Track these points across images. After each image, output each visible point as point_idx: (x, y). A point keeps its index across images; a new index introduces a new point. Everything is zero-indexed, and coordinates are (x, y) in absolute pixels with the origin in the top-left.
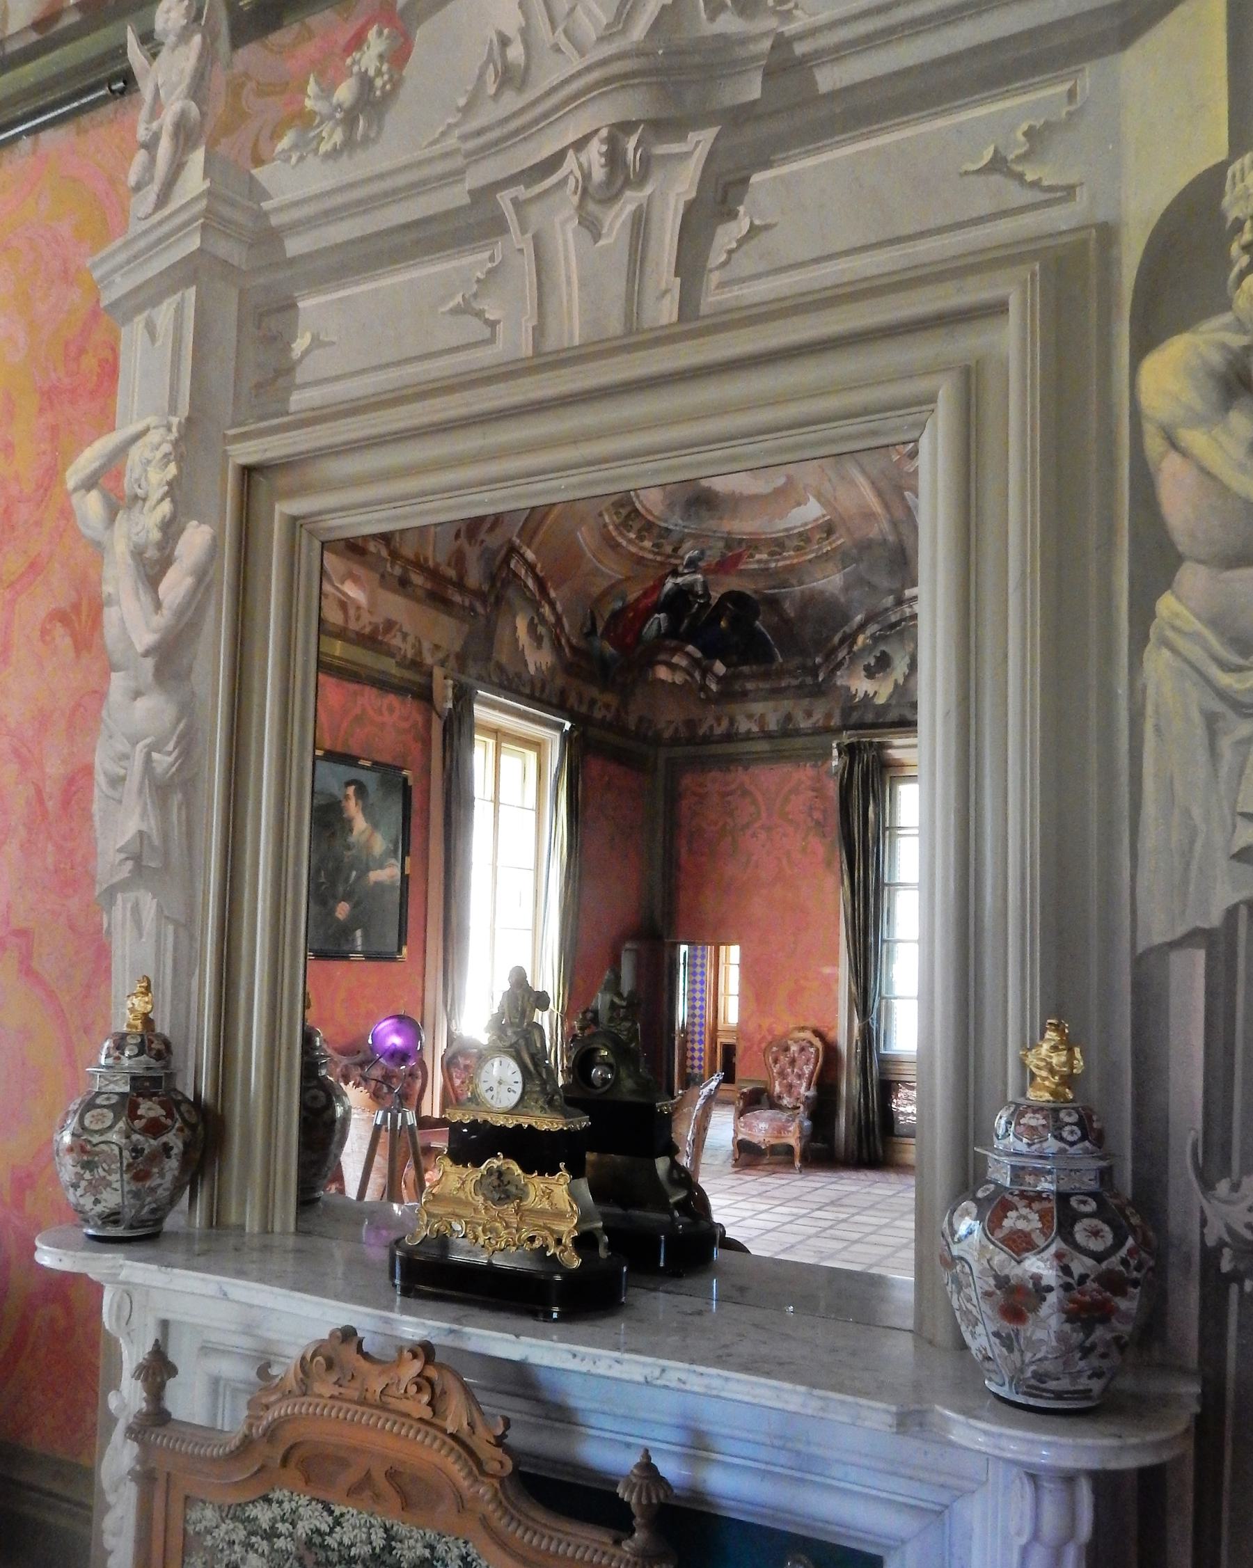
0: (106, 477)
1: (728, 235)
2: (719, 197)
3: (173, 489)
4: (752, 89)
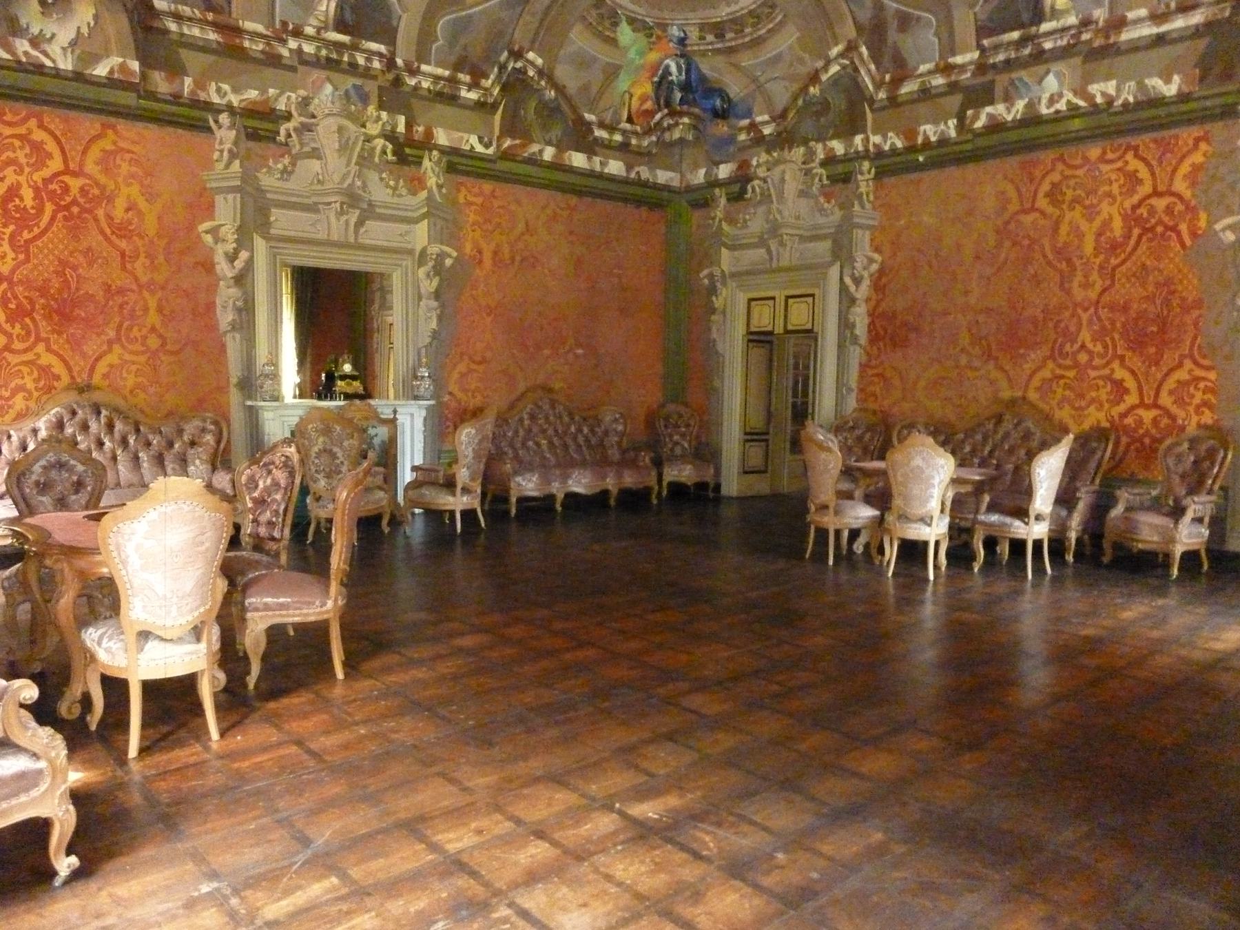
0: (214, 231)
1: (362, 230)
2: (360, 223)
3: (237, 241)
4: (365, 206)
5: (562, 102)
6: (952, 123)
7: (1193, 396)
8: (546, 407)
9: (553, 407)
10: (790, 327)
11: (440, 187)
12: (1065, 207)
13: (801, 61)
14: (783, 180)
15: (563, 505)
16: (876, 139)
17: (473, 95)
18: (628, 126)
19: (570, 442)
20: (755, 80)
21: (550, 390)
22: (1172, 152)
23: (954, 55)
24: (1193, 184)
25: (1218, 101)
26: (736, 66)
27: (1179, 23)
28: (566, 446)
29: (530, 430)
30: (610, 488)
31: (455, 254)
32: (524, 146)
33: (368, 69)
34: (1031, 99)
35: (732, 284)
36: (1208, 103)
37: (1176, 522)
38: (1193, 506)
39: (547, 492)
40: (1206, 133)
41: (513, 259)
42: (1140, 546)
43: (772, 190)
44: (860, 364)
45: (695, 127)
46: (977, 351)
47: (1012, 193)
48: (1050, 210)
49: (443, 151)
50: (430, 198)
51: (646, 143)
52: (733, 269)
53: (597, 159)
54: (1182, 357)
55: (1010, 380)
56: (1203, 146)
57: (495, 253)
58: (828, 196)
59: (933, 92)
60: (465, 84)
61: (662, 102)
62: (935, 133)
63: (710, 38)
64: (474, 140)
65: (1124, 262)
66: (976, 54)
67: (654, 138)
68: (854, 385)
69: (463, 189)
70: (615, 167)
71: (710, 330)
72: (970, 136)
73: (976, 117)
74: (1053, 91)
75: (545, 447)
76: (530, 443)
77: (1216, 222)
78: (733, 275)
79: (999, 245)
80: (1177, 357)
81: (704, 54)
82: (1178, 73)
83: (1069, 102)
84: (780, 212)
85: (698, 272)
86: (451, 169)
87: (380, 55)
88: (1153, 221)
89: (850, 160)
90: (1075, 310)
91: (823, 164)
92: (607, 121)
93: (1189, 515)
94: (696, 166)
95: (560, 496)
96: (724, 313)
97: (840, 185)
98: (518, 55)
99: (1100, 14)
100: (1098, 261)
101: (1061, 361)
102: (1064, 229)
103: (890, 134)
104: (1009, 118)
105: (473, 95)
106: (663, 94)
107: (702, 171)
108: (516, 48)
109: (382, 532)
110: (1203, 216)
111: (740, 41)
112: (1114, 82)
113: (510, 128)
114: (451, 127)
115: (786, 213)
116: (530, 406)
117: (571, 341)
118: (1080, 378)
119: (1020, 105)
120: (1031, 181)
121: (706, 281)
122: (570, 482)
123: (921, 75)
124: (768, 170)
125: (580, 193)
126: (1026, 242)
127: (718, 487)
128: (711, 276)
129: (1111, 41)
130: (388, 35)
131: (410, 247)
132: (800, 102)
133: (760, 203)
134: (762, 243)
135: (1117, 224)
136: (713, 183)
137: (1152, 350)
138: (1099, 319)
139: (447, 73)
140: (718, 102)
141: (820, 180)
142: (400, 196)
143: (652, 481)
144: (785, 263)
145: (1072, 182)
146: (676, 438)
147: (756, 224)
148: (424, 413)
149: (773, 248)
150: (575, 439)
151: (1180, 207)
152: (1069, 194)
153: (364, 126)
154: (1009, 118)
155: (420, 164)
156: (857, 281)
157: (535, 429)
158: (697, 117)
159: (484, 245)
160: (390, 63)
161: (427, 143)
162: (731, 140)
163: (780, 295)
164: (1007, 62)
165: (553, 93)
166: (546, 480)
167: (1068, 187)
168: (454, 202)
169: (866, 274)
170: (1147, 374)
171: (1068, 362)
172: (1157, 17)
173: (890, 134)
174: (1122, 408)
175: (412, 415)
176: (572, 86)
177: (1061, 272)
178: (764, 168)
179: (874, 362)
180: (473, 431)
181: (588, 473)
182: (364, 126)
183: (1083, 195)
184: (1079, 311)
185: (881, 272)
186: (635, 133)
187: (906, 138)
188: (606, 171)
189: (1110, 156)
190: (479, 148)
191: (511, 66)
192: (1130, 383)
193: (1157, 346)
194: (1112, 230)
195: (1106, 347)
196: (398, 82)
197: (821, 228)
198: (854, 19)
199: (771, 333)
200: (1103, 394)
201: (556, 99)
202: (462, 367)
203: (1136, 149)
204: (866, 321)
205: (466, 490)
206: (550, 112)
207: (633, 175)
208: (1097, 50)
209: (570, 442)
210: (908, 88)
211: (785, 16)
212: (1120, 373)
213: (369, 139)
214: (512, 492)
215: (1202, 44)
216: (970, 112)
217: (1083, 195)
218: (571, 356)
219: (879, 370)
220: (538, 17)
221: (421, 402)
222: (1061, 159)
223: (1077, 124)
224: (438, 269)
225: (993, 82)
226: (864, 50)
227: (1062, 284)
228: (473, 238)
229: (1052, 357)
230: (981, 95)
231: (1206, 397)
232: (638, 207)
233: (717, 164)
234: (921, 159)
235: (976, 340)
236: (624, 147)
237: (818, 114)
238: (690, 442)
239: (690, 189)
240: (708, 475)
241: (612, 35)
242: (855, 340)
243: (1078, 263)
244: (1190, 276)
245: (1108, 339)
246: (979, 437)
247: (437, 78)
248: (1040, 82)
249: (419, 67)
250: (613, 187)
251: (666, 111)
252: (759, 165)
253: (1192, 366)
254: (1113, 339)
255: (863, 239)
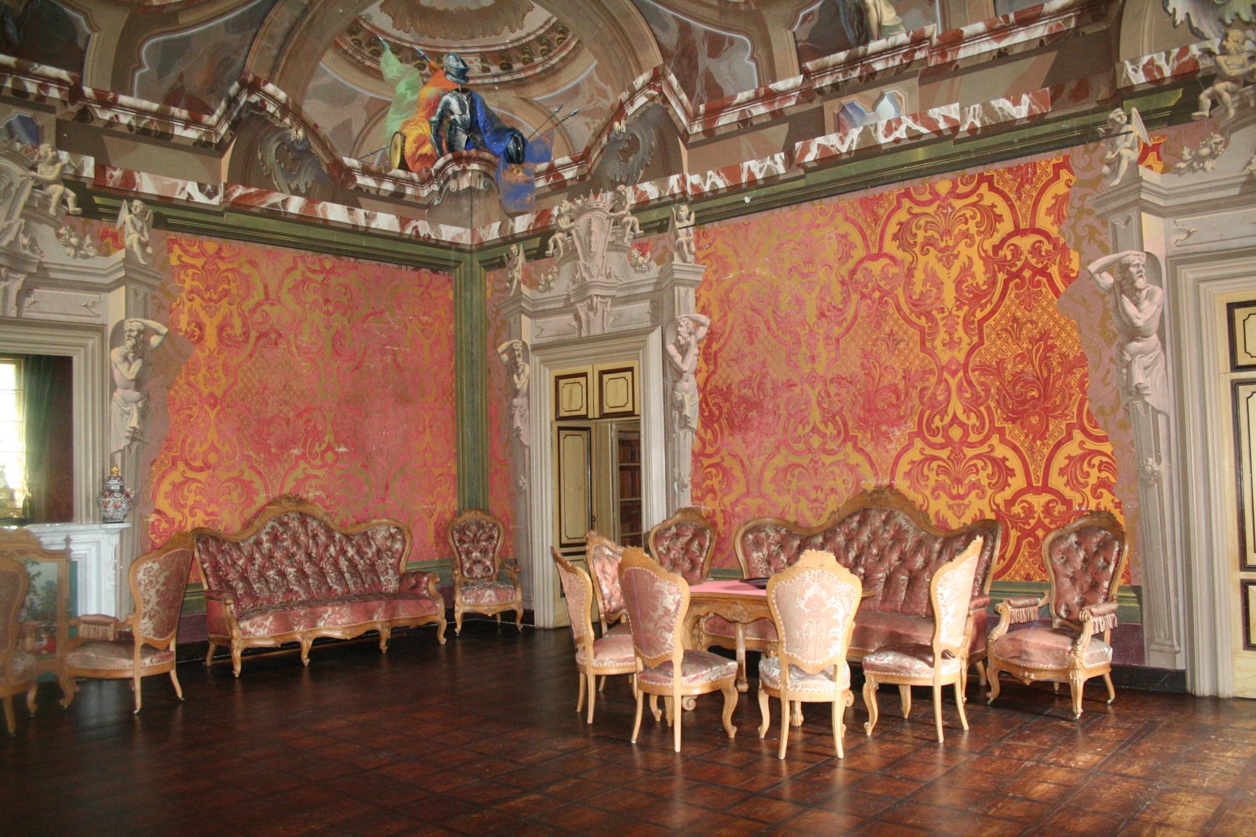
1: (28, 301)
2: (25, 292)
4: (34, 270)
5: (313, 145)
6: (780, 157)
7: (1088, 475)
8: (294, 524)
9: (304, 523)
10: (607, 410)
11: (143, 245)
12: (917, 250)
13: (602, 93)
14: (590, 233)
15: (310, 654)
16: (694, 179)
17: (192, 134)
18: (401, 173)
19: (328, 568)
20: (551, 117)
21: (301, 501)
22: (1029, 181)
23: (774, 80)
24: (1059, 220)
25: (1075, 122)
26: (528, 101)
27: (1020, 37)
28: (322, 574)
29: (271, 557)
30: (379, 627)
31: (164, 330)
32: (260, 195)
33: (40, 98)
34: (865, 128)
35: (535, 359)
36: (1065, 125)
37: (1074, 643)
38: (1092, 620)
39: (288, 640)
40: (1066, 158)
41: (246, 334)
42: (1033, 676)
43: (577, 244)
44: (694, 453)
45: (486, 175)
46: (831, 430)
47: (855, 237)
48: (900, 254)
49: (148, 201)
50: (129, 260)
51: (425, 193)
52: (537, 341)
53: (360, 213)
54: (1070, 427)
55: (872, 464)
56: (1064, 174)
57: (221, 329)
58: (643, 249)
59: (755, 123)
60: (180, 120)
61: (444, 145)
62: (761, 170)
63: (495, 69)
64: (192, 188)
65: (993, 312)
66: (800, 79)
67: (436, 188)
68: (687, 480)
69: (176, 248)
70: (385, 221)
71: (512, 417)
72: (801, 172)
73: (806, 150)
74: (889, 116)
75: (291, 577)
76: (271, 573)
77: (1089, 262)
78: (536, 348)
79: (846, 300)
80: (1064, 427)
81: (489, 88)
82: (1028, 93)
83: (908, 129)
84: (587, 269)
85: (496, 346)
86: (160, 222)
87: (59, 81)
88: (1019, 264)
89: (668, 204)
90: (941, 374)
91: (636, 210)
92: (374, 167)
93: (1089, 631)
94: (488, 221)
95: (307, 645)
96: (528, 395)
97: (655, 236)
98: (254, 87)
99: (933, 30)
100: (961, 313)
101: (933, 440)
102: (919, 276)
103: (710, 173)
104: (844, 149)
105: (192, 134)
106: (445, 135)
107: (496, 226)
108: (250, 78)
109: (438, 643)
110: (1074, 255)
111: (530, 73)
112: (957, 105)
113: (242, 173)
114: (154, 170)
115: (594, 272)
116: (270, 524)
117: (329, 438)
118: (956, 458)
119: (854, 134)
120: (876, 221)
121: (505, 357)
122: (321, 624)
123: (739, 105)
124: (572, 221)
125: (338, 253)
126: (877, 295)
127: (529, 616)
128: (511, 350)
129: (949, 59)
130: (74, 60)
131: (98, 321)
132: (605, 140)
133: (565, 260)
134: (568, 307)
135: (979, 268)
136: (509, 239)
137: (1034, 420)
138: (970, 383)
139: (155, 106)
140: (511, 145)
141: (632, 229)
142: (86, 257)
143: (438, 614)
144: (596, 330)
145: (922, 222)
146: (476, 554)
147: (561, 284)
148: (116, 539)
149: (582, 314)
150: (336, 564)
151: (1047, 246)
152: (921, 236)
153: (34, 168)
154: (844, 149)
155: (114, 217)
156: (683, 350)
157: (278, 555)
158: (488, 162)
159: (204, 318)
160: (75, 92)
161: (127, 191)
162: (529, 185)
163: (593, 371)
164: (835, 86)
165: (301, 133)
166: (285, 624)
167: (918, 227)
168: (165, 265)
169: (692, 340)
170: (1031, 449)
171: (939, 439)
172: (995, 32)
173: (710, 173)
174: (1008, 493)
175: (98, 543)
176: (327, 126)
177: (922, 330)
178: (567, 219)
179: (709, 450)
180: (156, 566)
181: (346, 610)
182: (34, 168)
183: (937, 236)
184: (946, 375)
185: (711, 337)
186: (411, 181)
187: (728, 177)
188: (373, 225)
189: (962, 189)
190: (200, 198)
191: (243, 100)
192: (1014, 462)
193: (1039, 415)
194: (973, 276)
195: (980, 417)
196: (85, 115)
197: (637, 287)
198: (658, 43)
199: (585, 417)
200: (983, 478)
201: (305, 139)
202: (176, 476)
203: (990, 180)
204: (697, 399)
205: (149, 649)
206: (296, 156)
207: (408, 231)
208: (934, 70)
209: (328, 568)
210: (726, 119)
211: (579, 42)
212: (1001, 451)
213: (40, 185)
214: (235, 643)
215: (1051, 57)
216: (798, 145)
217: (937, 236)
218: (330, 457)
219: (716, 460)
220: (279, 40)
221: (110, 526)
222: (907, 194)
223: (920, 154)
224: (141, 349)
225: (821, 109)
226: (673, 78)
227: (923, 343)
228: (190, 311)
229: (919, 433)
230: (812, 125)
231: (1104, 474)
232: (417, 269)
233: (513, 216)
234: (747, 200)
235: (830, 417)
236: (396, 198)
237: (625, 154)
238: (493, 560)
239: (482, 247)
240: (515, 601)
241: (374, 66)
242: (685, 421)
243: (939, 316)
244: (1069, 328)
245: (982, 409)
246: (841, 539)
247: (141, 112)
248: (874, 108)
249: (115, 99)
250: (381, 244)
251: (450, 156)
252: (560, 216)
253: (1084, 438)
254: (988, 408)
255: (686, 297)
